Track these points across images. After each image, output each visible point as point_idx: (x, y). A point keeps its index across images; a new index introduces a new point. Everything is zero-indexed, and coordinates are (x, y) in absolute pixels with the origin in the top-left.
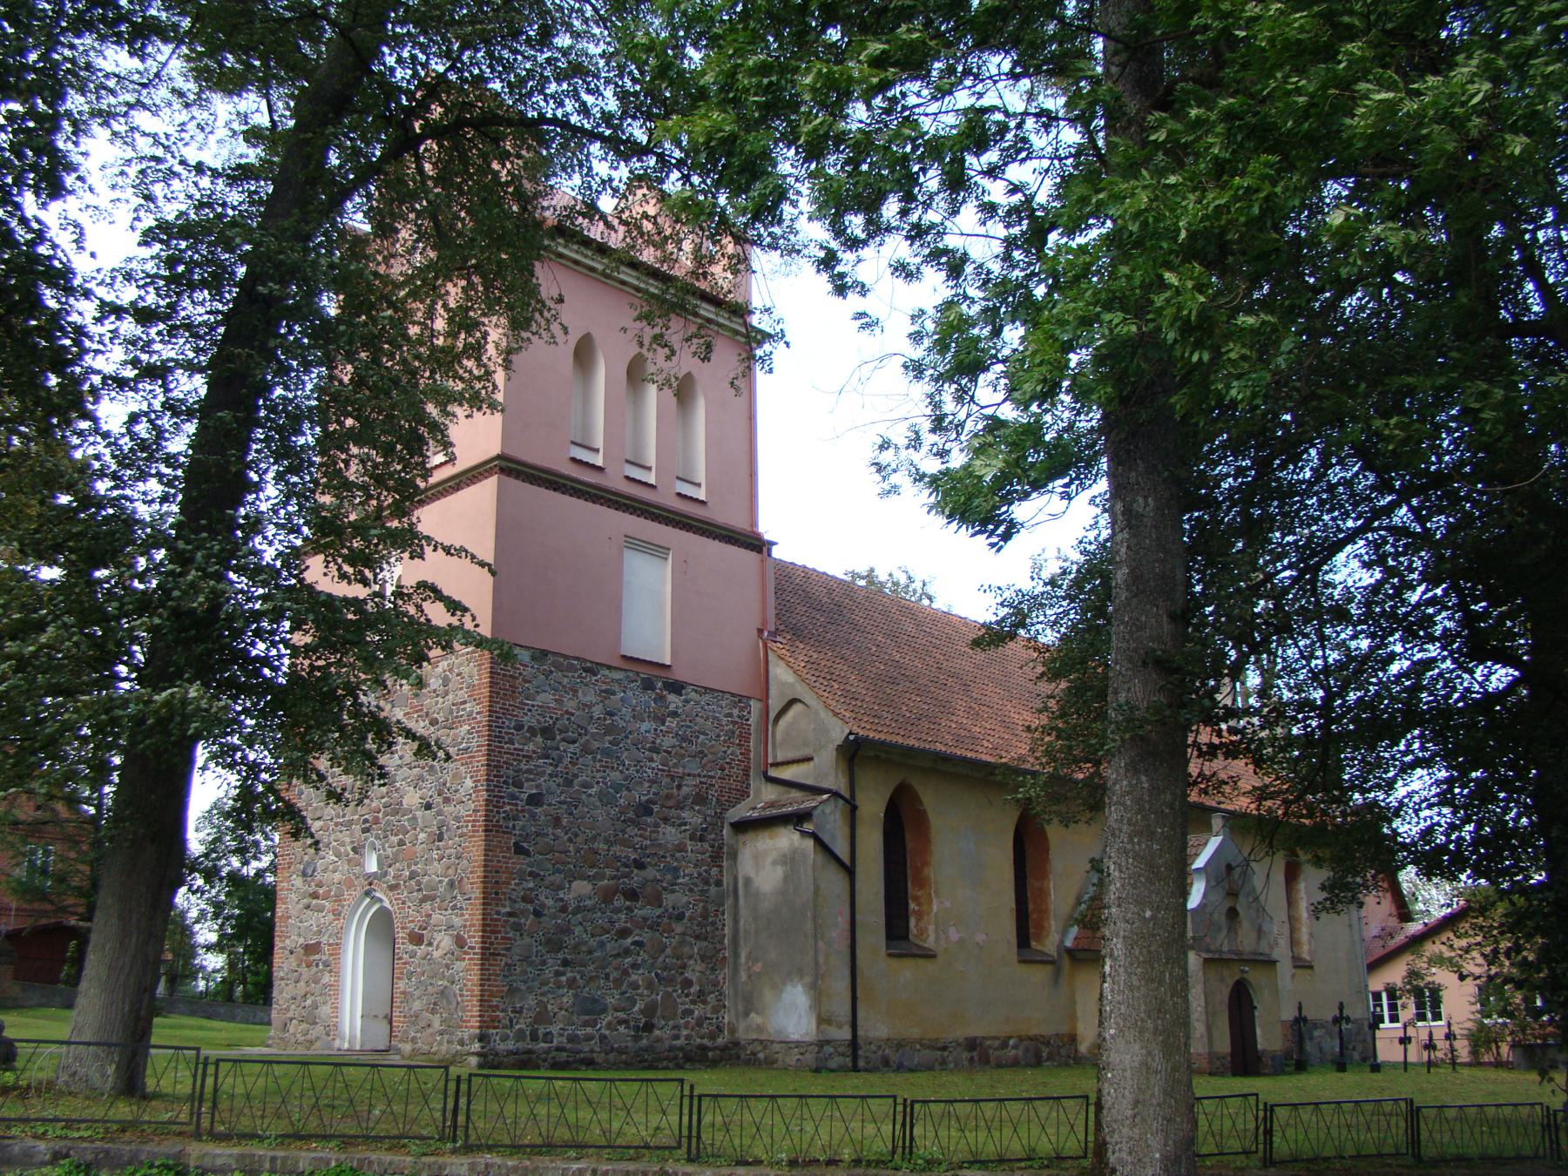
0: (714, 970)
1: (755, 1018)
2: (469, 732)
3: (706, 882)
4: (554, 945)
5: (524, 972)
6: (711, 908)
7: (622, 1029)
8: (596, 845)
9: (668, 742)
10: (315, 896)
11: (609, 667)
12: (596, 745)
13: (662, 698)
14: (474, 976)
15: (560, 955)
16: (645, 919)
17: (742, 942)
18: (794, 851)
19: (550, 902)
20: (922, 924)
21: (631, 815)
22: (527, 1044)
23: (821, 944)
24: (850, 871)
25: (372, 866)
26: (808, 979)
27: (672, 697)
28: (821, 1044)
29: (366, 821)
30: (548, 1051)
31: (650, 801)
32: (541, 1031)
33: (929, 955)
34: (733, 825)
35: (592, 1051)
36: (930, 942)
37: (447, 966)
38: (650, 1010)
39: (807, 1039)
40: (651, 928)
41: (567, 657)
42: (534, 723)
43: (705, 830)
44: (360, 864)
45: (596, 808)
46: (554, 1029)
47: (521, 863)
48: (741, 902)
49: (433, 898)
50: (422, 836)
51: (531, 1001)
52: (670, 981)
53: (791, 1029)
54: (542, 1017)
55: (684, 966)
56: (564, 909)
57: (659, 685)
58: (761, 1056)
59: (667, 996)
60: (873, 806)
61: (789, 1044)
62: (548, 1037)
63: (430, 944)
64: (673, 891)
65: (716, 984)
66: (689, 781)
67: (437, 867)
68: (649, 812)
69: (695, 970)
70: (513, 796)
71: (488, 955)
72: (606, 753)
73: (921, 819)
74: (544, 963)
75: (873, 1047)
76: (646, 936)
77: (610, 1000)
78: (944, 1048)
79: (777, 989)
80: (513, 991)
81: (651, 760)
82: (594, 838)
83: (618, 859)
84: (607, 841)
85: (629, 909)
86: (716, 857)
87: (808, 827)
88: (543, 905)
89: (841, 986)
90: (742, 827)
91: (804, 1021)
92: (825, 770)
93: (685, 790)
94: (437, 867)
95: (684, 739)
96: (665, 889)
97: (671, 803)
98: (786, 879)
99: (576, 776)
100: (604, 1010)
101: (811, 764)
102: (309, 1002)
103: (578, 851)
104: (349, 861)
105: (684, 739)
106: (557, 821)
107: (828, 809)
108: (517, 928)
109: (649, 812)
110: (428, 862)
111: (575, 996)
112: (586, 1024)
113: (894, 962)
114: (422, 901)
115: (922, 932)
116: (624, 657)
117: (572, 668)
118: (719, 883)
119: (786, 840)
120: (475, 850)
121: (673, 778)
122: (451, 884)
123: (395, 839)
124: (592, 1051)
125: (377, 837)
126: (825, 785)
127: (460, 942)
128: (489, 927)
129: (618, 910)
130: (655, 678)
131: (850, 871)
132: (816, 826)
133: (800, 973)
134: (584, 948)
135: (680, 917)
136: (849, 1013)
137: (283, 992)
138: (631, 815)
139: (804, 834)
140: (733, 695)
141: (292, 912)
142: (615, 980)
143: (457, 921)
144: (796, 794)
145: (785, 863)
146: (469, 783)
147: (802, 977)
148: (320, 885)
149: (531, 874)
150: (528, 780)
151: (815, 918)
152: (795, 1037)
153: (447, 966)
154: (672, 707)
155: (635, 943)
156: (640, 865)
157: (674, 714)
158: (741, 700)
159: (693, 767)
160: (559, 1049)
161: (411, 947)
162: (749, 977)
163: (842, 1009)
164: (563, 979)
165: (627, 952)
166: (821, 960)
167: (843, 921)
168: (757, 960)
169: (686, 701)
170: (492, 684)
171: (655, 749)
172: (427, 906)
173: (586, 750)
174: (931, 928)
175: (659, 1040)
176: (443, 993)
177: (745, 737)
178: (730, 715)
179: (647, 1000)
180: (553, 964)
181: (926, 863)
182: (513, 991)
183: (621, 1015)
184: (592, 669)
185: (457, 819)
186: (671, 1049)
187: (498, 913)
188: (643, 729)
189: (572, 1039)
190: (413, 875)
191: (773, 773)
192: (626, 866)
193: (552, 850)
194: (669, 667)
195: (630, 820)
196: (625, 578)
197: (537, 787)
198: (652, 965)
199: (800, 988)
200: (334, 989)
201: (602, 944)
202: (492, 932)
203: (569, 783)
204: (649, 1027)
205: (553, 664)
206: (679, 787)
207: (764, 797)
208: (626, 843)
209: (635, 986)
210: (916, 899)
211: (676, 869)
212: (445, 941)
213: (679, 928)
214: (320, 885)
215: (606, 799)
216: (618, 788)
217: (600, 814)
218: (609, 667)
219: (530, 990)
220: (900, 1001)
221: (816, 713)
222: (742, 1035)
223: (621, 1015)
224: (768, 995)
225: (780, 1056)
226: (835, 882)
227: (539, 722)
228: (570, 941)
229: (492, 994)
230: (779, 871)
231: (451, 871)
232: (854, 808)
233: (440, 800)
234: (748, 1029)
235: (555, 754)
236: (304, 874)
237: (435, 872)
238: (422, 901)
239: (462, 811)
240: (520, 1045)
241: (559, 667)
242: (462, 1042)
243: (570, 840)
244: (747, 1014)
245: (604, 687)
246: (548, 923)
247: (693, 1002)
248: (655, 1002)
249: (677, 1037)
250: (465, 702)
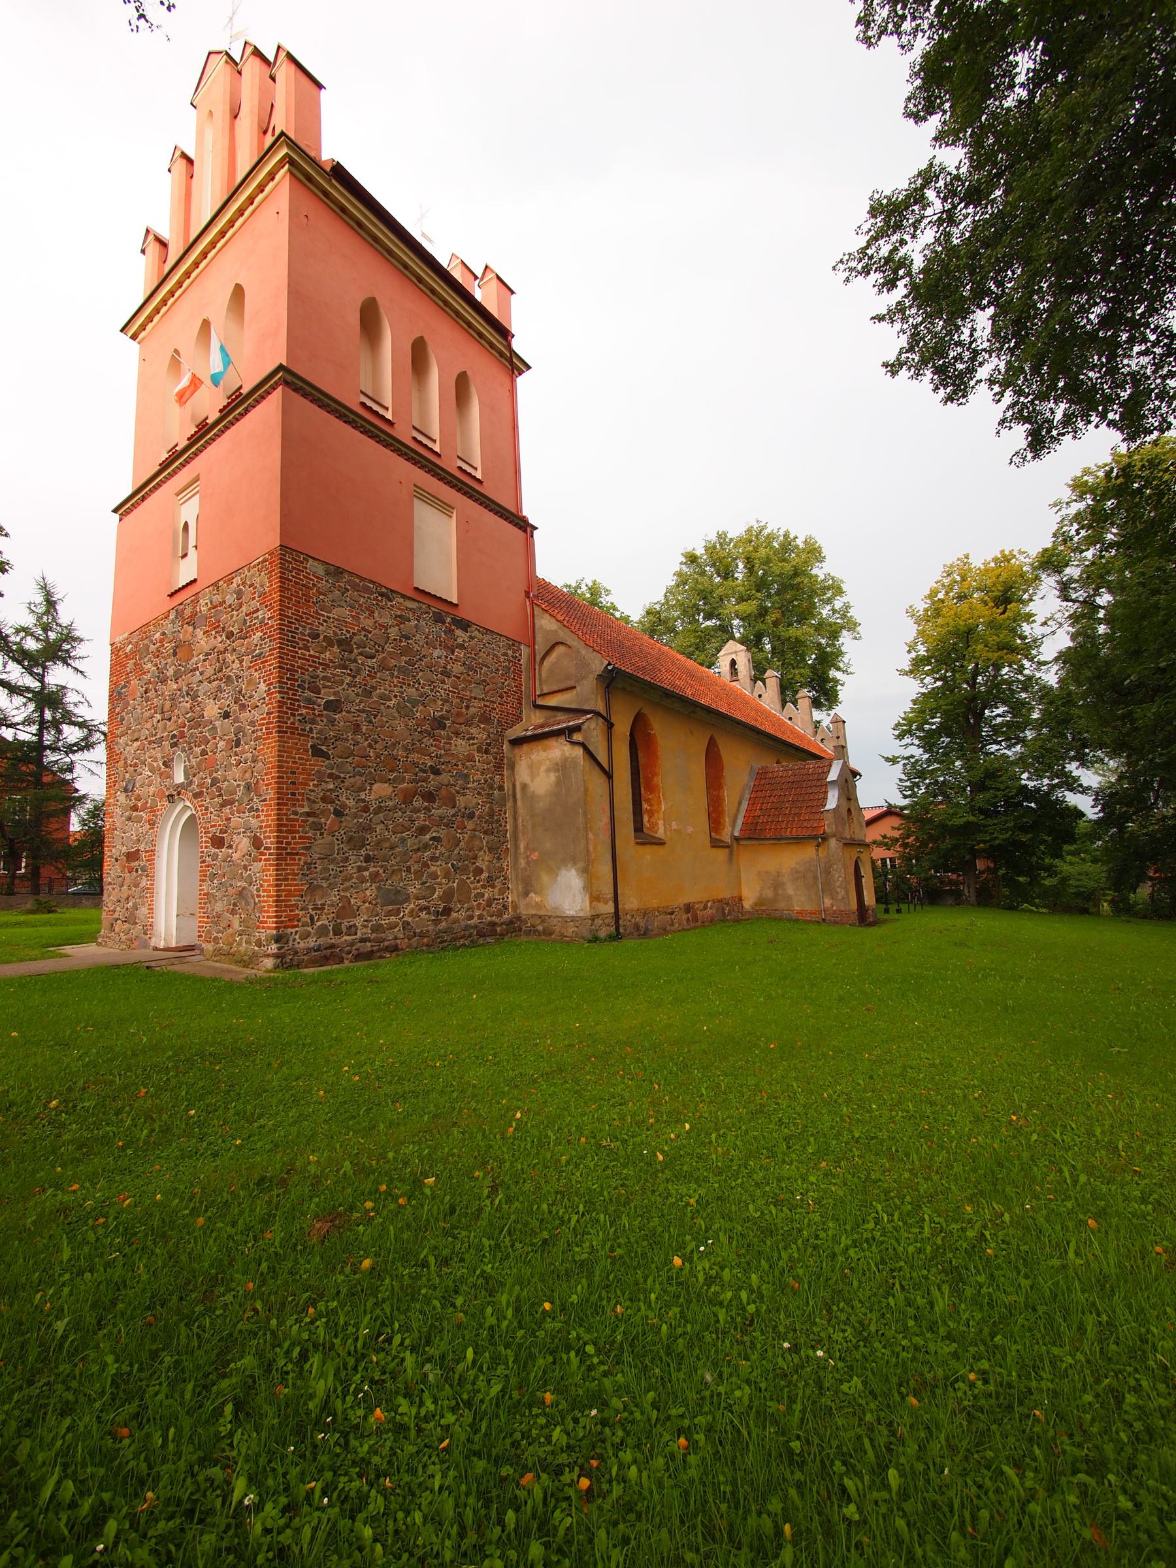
0: (499, 859)
1: (534, 898)
2: (262, 639)
3: (491, 788)
4: (356, 842)
5: (326, 870)
6: (496, 808)
7: (423, 915)
8: (395, 752)
9: (457, 669)
10: (135, 808)
11: (404, 596)
12: (394, 662)
13: (451, 631)
14: (270, 875)
15: (363, 852)
16: (442, 818)
17: (520, 835)
18: (565, 760)
19: (351, 803)
20: (653, 820)
21: (427, 727)
22: (331, 939)
23: (591, 835)
24: (609, 775)
25: (179, 777)
26: (580, 865)
27: (459, 632)
28: (594, 918)
29: (174, 736)
30: (352, 944)
31: (442, 717)
32: (345, 924)
33: (661, 843)
34: (510, 741)
35: (396, 938)
36: (661, 833)
37: (245, 867)
38: (448, 896)
39: (581, 914)
40: (447, 825)
41: (362, 579)
42: (330, 633)
43: (489, 744)
44: (170, 777)
45: (395, 718)
46: (358, 922)
47: (321, 765)
48: (519, 803)
49: (231, 802)
50: (221, 744)
51: (333, 897)
52: (465, 870)
53: (566, 906)
54: (346, 910)
55: (475, 857)
56: (366, 809)
57: (449, 619)
58: (540, 928)
59: (462, 883)
60: (623, 727)
61: (566, 920)
62: (352, 930)
63: (230, 847)
64: (464, 794)
65: (501, 870)
66: (475, 703)
67: (235, 772)
68: (444, 727)
69: (484, 860)
70: (309, 701)
71: (284, 854)
72: (402, 670)
73: (650, 741)
74: (346, 859)
75: (629, 917)
76: (443, 833)
77: (412, 890)
78: (672, 913)
79: (554, 872)
80: (313, 889)
81: (443, 682)
82: (394, 745)
83: (416, 765)
84: (405, 748)
85: (427, 809)
86: (499, 767)
87: (577, 737)
88: (344, 806)
89: (605, 869)
90: (517, 742)
91: (579, 899)
92: (586, 693)
93: (472, 710)
94: (235, 772)
95: (470, 669)
96: (458, 792)
97: (461, 720)
98: (558, 783)
99: (375, 688)
100: (407, 900)
101: (574, 692)
102: (131, 904)
103: (378, 756)
104: (161, 775)
105: (470, 669)
106: (357, 728)
107: (593, 725)
108: (318, 827)
109: (444, 727)
110: (227, 768)
111: (378, 888)
112: (389, 914)
113: (640, 848)
114: (223, 805)
115: (654, 826)
116: (417, 589)
117: (367, 590)
118: (501, 788)
119: (559, 750)
120: (269, 751)
121: (462, 700)
122: (248, 787)
123: (198, 750)
124: (396, 938)
125: (183, 750)
126: (586, 707)
127: (257, 843)
128: (283, 827)
129: (418, 811)
130: (442, 612)
131: (609, 775)
132: (584, 738)
133: (574, 860)
134: (387, 845)
135: (471, 816)
136: (612, 891)
137: (111, 895)
138: (427, 727)
139: (573, 743)
140: (508, 639)
141: (117, 824)
142: (416, 872)
143: (254, 822)
144: (561, 716)
145: (558, 771)
146: (263, 687)
147: (575, 863)
148: (139, 798)
149: (330, 775)
150: (325, 687)
151: (585, 814)
152: (572, 913)
153: (245, 867)
154: (460, 640)
155: (433, 839)
156: (437, 772)
157: (462, 647)
158: (514, 643)
159: (478, 692)
160: (363, 940)
161: (214, 850)
162: (528, 863)
163: (608, 891)
164: (366, 873)
165: (426, 847)
166: (591, 849)
167: (606, 819)
168: (534, 850)
169: (471, 638)
170: (283, 589)
171: (446, 673)
172: (227, 810)
173: (383, 667)
174: (661, 822)
175: (457, 921)
176: (241, 894)
177: (518, 673)
178: (506, 654)
179: (445, 887)
180: (355, 861)
181: (655, 774)
182: (313, 889)
183: (422, 902)
184: (388, 595)
185: (252, 723)
186: (467, 928)
187: (295, 813)
188: (435, 654)
189: (377, 928)
190: (215, 781)
191: (540, 702)
192: (424, 772)
193: (351, 754)
194: (456, 605)
195: (426, 731)
196: (416, 523)
197: (335, 694)
198: (449, 857)
199: (573, 872)
200: (150, 891)
201: (403, 840)
202: (288, 832)
203: (368, 694)
204: (447, 911)
205: (348, 582)
206: (467, 707)
207: (532, 721)
208: (423, 752)
209: (434, 876)
210: (648, 801)
211: (467, 776)
212: (244, 844)
213: (470, 825)
214: (139, 798)
215: (404, 711)
216: (415, 703)
217: (399, 725)
218: (404, 596)
219: (331, 886)
220: (652, 883)
221: (578, 651)
222: (524, 911)
223: (422, 902)
224: (545, 878)
225: (557, 929)
226: (597, 783)
227: (335, 634)
228: (371, 838)
229: (290, 894)
230: (553, 777)
231: (248, 775)
232: (610, 726)
233: (236, 707)
234: (528, 906)
235: (353, 666)
236: (126, 790)
237: (234, 778)
238: (223, 805)
239: (256, 715)
240: (321, 941)
241: (355, 587)
242: (259, 943)
243: (370, 746)
244: (526, 894)
245: (399, 613)
246: (349, 822)
247: (484, 887)
248: (452, 888)
249: (471, 917)
250: (257, 610)
